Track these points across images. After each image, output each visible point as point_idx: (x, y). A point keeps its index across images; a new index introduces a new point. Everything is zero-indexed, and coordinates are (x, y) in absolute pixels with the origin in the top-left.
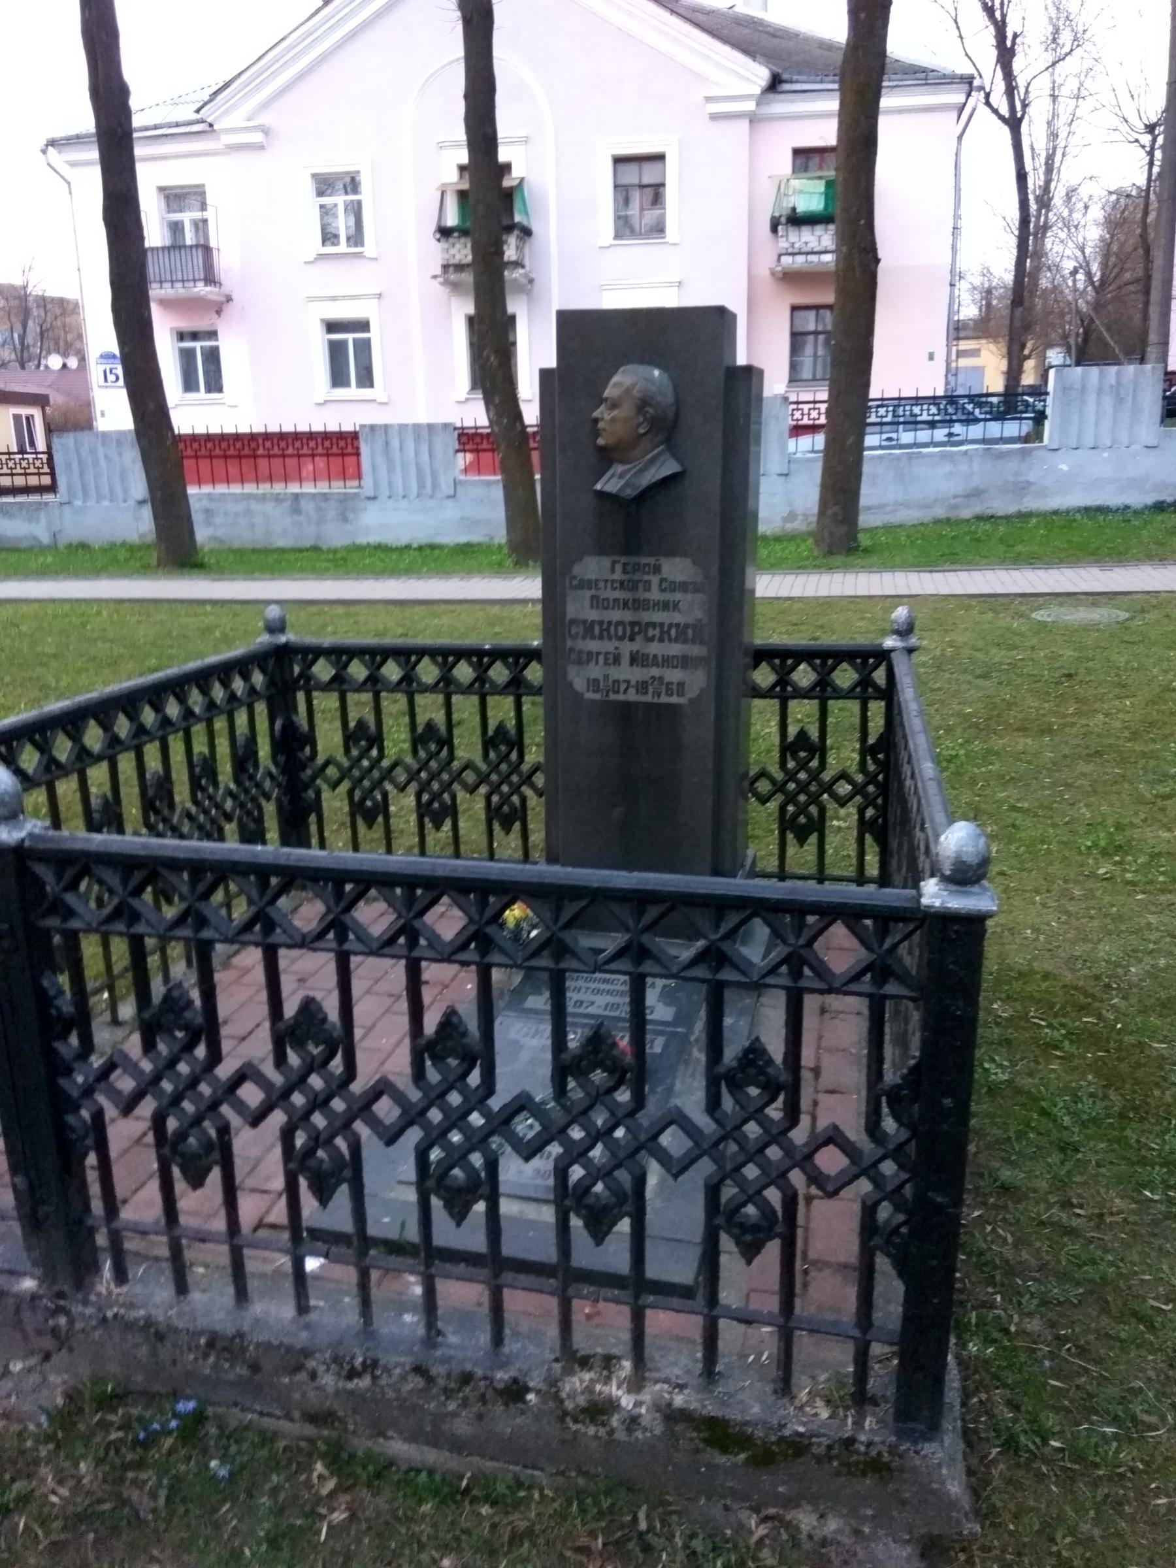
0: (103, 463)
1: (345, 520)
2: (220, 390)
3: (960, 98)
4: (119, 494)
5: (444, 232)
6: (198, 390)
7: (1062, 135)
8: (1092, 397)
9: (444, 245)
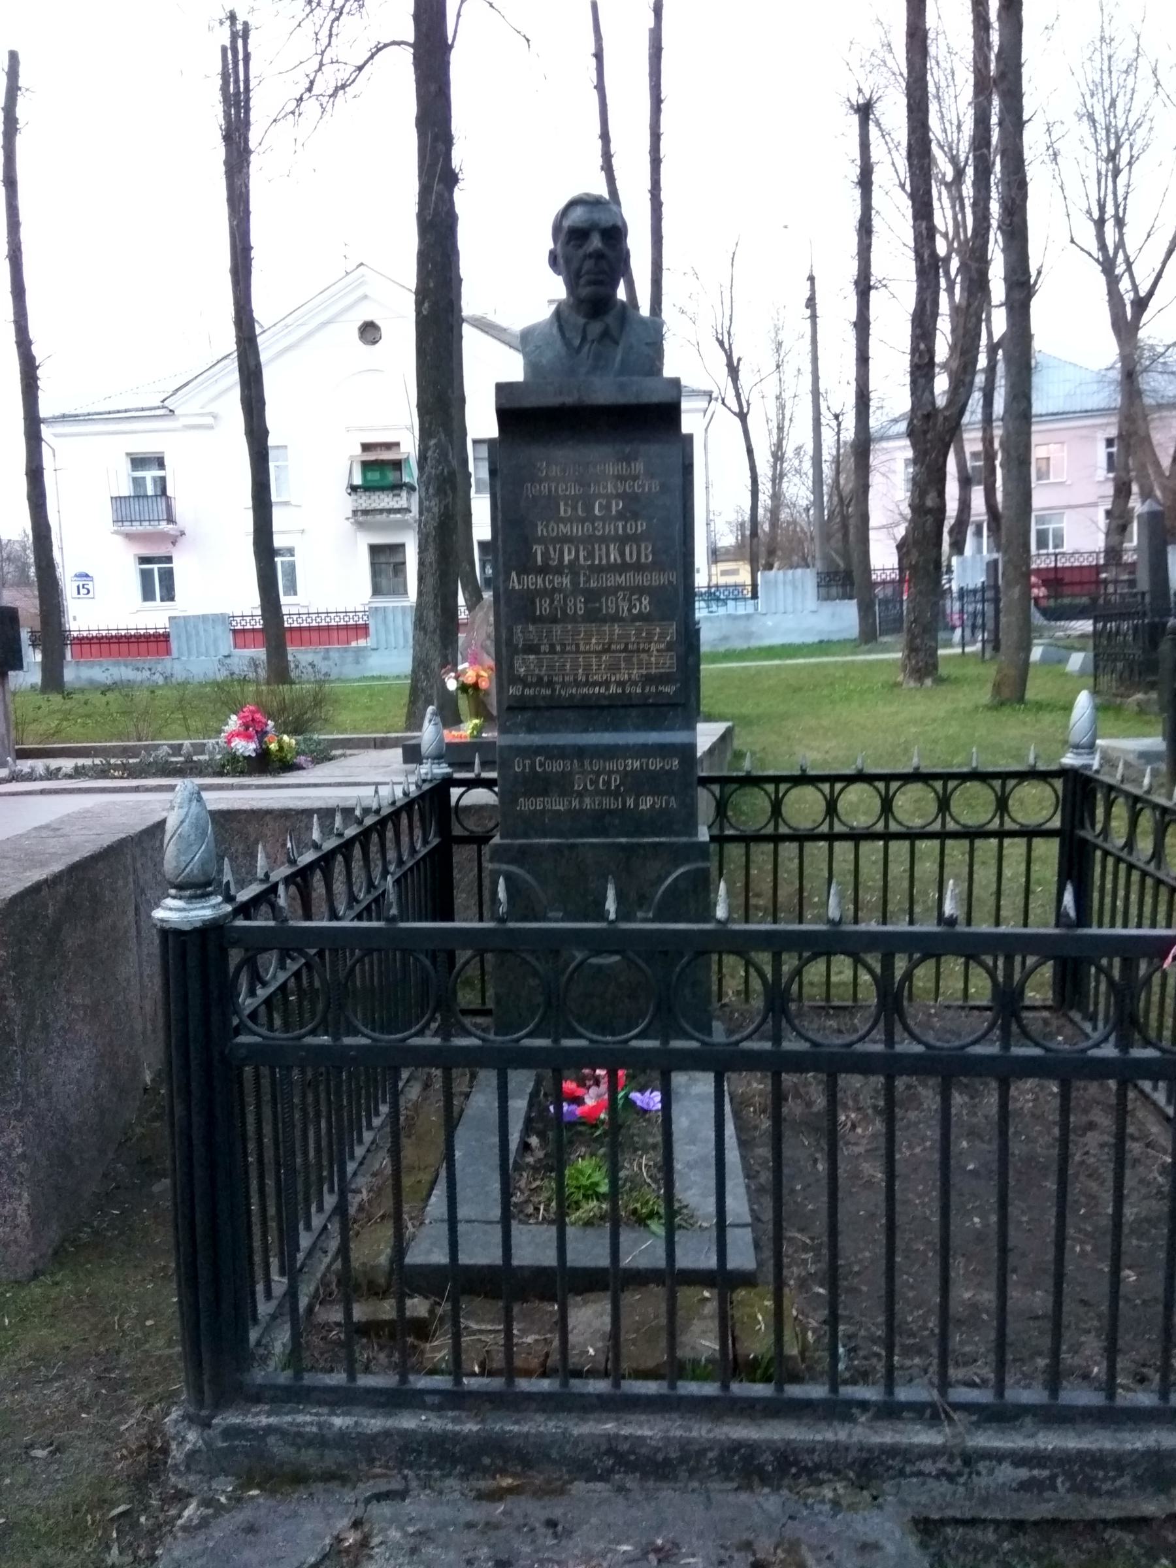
0: (202, 633)
1: (358, 662)
2: (172, 599)
3: (704, 404)
4: (212, 652)
5: (354, 489)
6: (153, 599)
7: (788, 405)
8: (781, 587)
9: (354, 497)
